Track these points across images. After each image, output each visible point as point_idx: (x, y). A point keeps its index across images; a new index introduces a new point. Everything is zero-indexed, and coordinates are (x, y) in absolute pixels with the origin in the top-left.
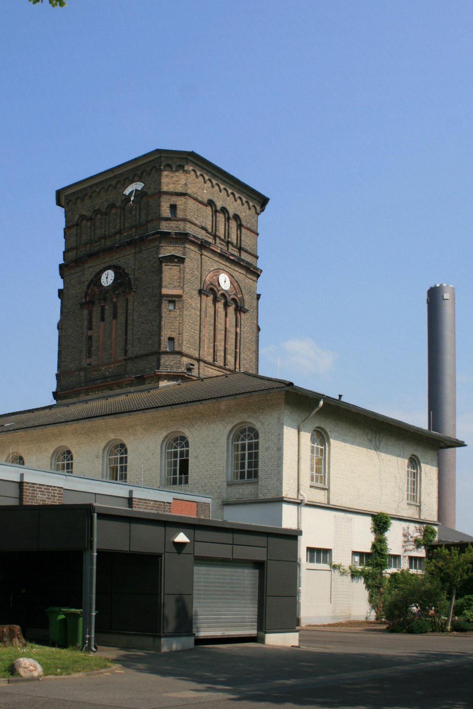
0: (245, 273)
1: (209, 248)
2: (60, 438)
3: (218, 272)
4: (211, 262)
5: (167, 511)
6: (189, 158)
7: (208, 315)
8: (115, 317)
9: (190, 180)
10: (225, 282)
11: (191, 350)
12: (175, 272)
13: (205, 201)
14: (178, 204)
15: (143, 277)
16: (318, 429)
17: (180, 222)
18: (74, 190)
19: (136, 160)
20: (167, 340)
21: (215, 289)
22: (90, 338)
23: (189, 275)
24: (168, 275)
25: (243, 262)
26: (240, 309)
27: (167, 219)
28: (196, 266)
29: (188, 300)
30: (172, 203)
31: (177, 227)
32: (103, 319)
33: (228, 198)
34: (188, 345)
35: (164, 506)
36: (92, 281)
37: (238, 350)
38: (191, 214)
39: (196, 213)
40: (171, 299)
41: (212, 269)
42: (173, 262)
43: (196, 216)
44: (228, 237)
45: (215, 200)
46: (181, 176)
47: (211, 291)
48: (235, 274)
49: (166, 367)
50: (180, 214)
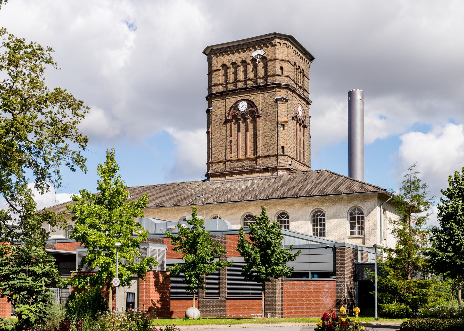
2: (247, 208)
6: (289, 39)
15: (266, 109)
17: (285, 78)
19: (261, 36)
20: (281, 148)
26: (305, 127)
27: (279, 75)
31: (284, 80)
36: (232, 106)
40: (282, 123)
42: (283, 101)
50: (285, 73)
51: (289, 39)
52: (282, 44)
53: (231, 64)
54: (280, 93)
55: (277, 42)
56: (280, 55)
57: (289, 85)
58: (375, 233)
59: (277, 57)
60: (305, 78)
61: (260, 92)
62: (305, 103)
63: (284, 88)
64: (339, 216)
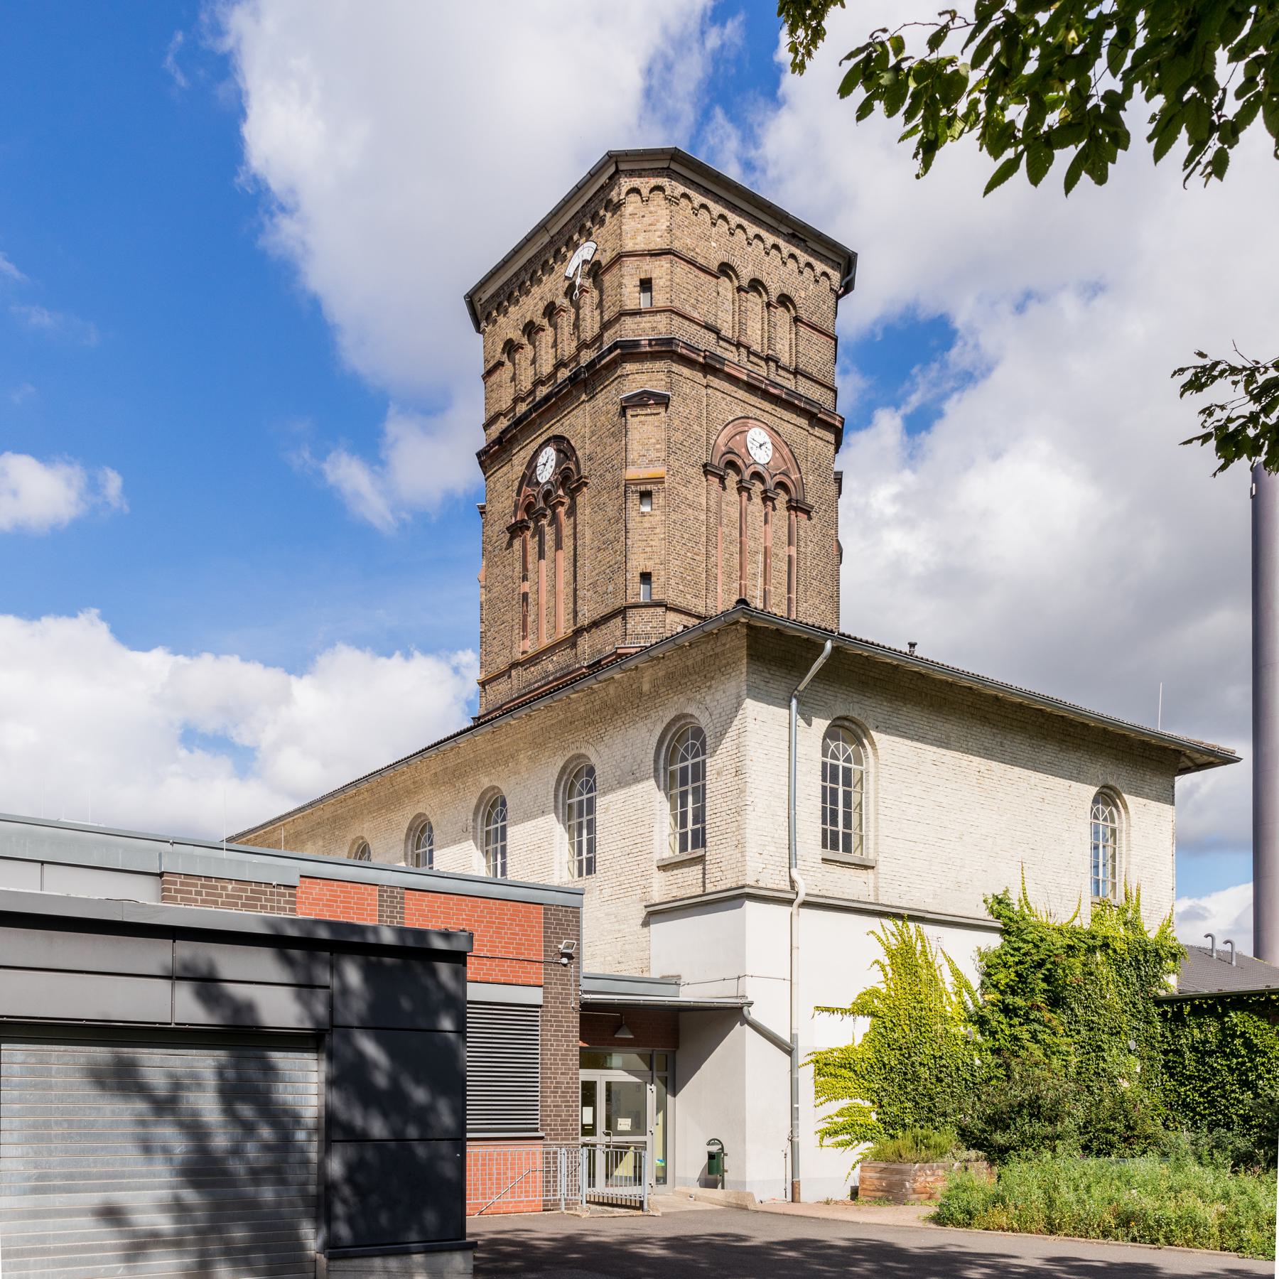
0: (806, 426)
1: (721, 371)
3: (745, 425)
4: (727, 403)
5: (284, 909)
6: (674, 166)
7: (725, 521)
8: (558, 546)
9: (678, 218)
10: (760, 447)
11: (688, 596)
12: (650, 428)
13: (714, 266)
14: (654, 276)
15: (599, 449)
16: (838, 723)
17: (658, 317)
18: (491, 290)
20: (638, 579)
21: (740, 462)
22: (525, 596)
23: (679, 434)
24: (637, 436)
25: (800, 400)
28: (695, 412)
29: (679, 487)
30: (643, 277)
32: (541, 555)
33: (767, 259)
34: (681, 587)
35: (272, 894)
37: (793, 596)
38: (683, 296)
39: (695, 295)
40: (643, 488)
41: (731, 418)
42: (646, 405)
43: (693, 301)
44: (769, 348)
45: (736, 262)
46: (660, 212)
47: (726, 467)
48: (785, 428)
49: (638, 636)
51: (674, 166)
52: (645, 192)
53: (524, 332)
54: (638, 377)
55: (624, 190)
56: (640, 238)
57: (670, 341)
58: (739, 828)
59: (629, 246)
60: (803, 330)
61: (584, 397)
62: (803, 422)
63: (654, 356)
64: (629, 778)
